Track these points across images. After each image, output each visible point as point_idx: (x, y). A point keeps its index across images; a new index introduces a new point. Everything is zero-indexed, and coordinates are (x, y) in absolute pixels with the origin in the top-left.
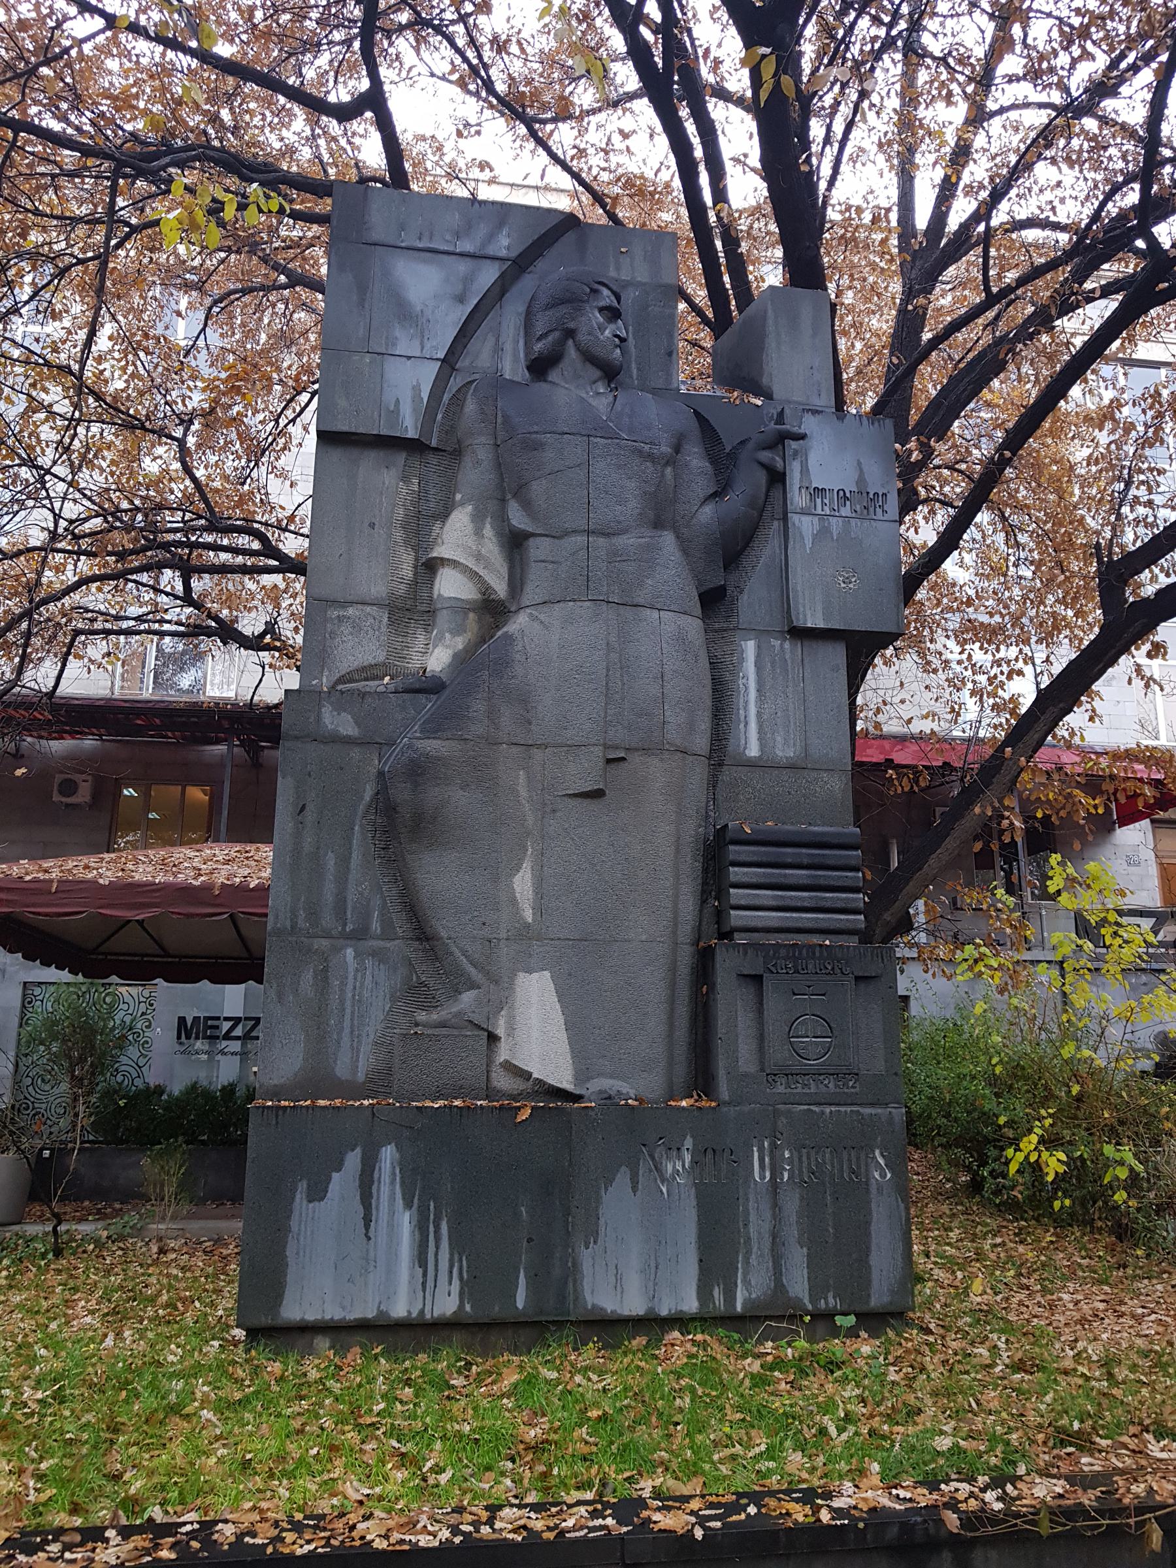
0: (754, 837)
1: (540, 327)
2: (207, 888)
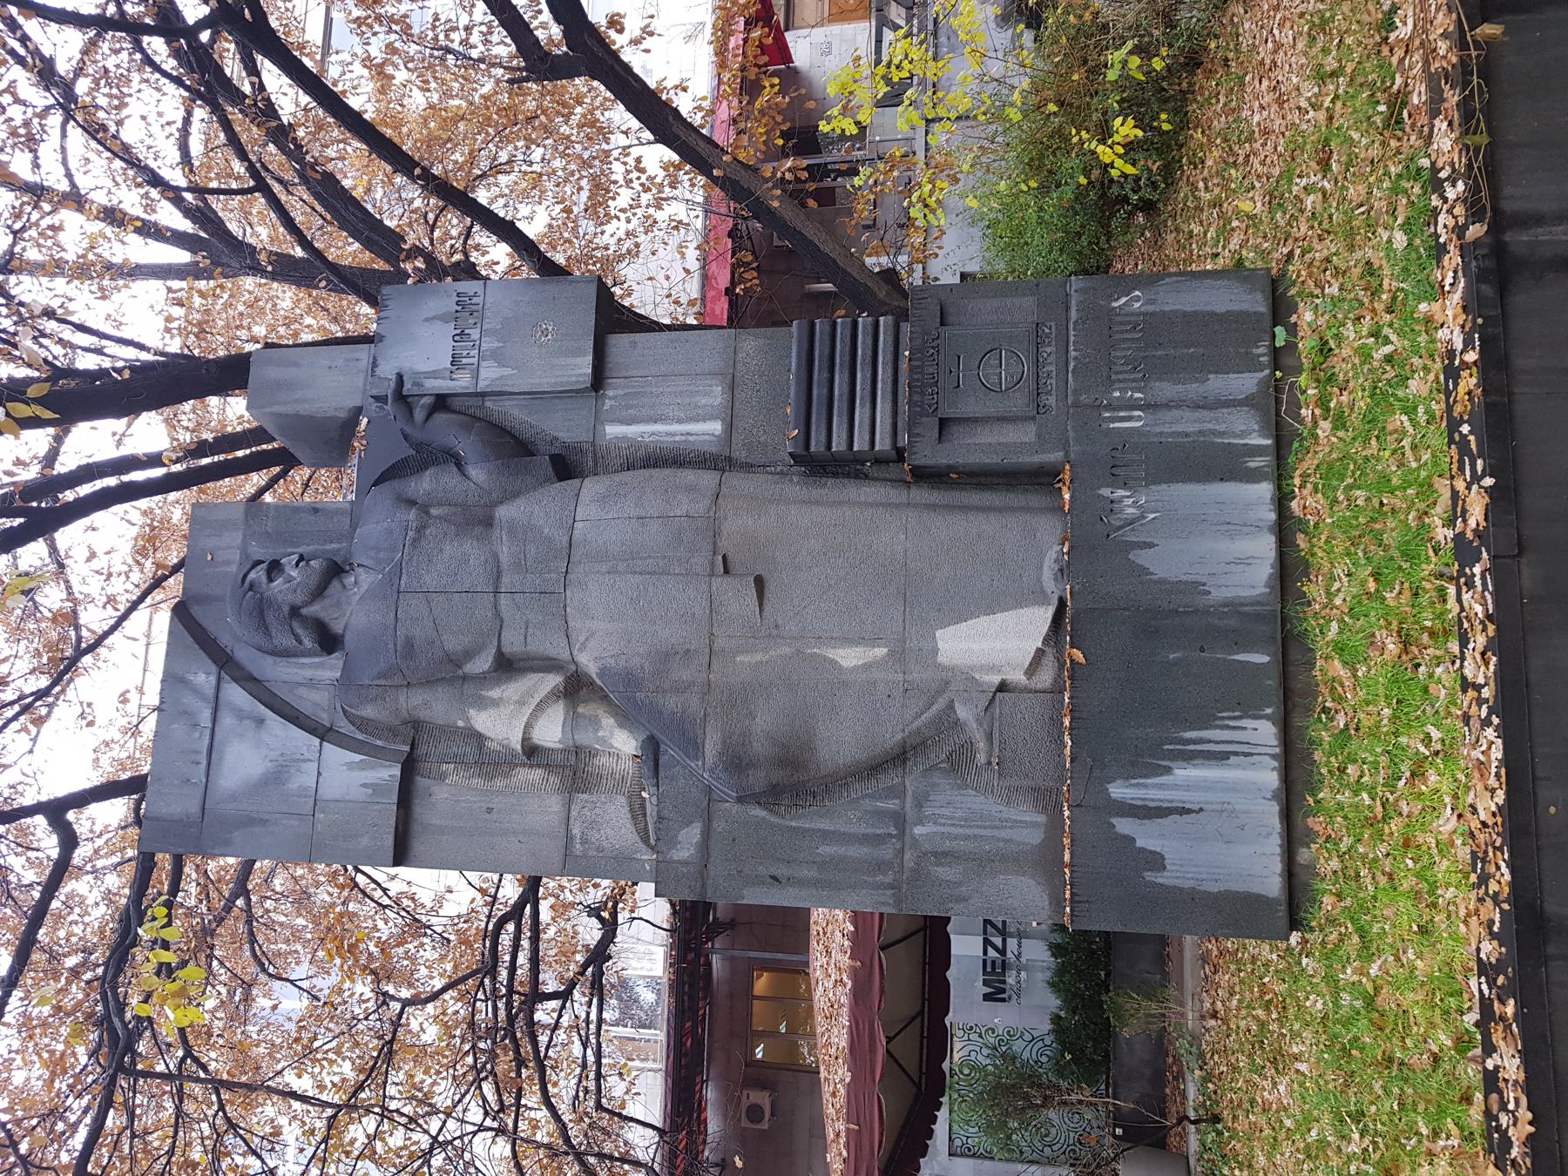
0: (802, 427)
1: (288, 642)
2: (855, 974)
